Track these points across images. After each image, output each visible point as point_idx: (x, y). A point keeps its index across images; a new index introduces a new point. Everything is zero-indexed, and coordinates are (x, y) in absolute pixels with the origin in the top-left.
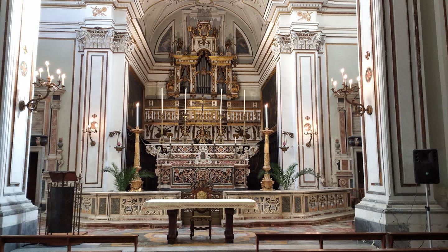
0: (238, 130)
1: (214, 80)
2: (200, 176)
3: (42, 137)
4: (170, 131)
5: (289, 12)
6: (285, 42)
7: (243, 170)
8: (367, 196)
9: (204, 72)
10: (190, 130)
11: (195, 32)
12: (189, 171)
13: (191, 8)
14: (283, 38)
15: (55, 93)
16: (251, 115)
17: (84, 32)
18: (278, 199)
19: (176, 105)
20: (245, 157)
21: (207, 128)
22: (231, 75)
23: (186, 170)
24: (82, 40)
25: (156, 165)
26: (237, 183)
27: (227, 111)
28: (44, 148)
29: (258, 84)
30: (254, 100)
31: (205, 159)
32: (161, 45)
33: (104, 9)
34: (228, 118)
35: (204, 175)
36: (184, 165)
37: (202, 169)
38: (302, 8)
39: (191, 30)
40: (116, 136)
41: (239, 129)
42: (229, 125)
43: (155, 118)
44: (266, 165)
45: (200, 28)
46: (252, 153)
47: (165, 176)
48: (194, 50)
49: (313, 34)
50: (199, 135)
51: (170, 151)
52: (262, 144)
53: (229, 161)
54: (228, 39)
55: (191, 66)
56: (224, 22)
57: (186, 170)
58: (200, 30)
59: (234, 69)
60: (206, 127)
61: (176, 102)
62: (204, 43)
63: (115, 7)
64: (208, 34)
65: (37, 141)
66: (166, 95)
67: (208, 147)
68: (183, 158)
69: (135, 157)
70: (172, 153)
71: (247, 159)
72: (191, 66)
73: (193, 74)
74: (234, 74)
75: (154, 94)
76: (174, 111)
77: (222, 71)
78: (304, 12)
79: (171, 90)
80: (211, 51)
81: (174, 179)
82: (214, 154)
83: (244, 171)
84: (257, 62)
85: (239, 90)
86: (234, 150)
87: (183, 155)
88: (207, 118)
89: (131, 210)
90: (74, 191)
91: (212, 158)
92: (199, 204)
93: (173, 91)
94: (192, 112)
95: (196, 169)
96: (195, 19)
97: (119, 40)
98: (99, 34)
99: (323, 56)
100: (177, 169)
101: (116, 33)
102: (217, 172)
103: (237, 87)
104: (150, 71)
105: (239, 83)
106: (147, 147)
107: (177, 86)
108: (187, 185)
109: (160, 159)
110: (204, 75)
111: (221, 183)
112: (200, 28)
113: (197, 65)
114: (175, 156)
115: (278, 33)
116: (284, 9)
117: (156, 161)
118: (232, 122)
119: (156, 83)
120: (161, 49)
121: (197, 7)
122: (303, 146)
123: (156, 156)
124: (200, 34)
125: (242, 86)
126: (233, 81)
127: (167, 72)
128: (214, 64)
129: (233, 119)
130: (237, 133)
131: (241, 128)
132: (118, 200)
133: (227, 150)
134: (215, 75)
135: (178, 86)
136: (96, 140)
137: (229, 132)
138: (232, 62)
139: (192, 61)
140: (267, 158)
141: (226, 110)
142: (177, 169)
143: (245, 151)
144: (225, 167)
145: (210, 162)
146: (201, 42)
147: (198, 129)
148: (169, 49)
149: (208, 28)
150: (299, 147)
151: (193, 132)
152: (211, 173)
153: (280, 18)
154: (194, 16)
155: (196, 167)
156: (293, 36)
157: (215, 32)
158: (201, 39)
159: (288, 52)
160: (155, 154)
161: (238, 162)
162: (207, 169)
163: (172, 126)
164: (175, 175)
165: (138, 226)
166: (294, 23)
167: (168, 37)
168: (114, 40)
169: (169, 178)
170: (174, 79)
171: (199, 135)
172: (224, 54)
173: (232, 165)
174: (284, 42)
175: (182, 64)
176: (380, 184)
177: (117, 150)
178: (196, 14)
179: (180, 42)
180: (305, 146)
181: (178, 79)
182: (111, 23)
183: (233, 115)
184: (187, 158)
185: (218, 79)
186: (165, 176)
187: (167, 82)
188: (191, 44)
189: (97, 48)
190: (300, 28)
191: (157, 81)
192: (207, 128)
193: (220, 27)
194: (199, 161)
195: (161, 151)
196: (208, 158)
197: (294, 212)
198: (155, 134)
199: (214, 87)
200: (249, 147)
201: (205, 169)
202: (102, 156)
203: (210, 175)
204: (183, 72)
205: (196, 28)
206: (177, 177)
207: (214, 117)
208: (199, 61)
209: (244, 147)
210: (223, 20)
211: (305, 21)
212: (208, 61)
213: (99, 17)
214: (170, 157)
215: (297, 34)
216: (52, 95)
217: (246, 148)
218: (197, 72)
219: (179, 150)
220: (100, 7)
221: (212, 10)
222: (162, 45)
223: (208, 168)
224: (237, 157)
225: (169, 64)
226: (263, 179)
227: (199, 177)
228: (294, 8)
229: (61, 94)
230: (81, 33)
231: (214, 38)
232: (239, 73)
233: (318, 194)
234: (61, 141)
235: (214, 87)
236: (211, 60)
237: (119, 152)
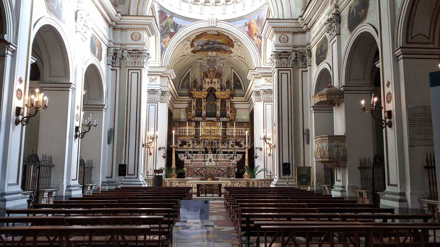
1: (218, 108)
2: (209, 172)
5: (260, 78)
6: (258, 95)
7: (233, 169)
10: (202, 141)
11: (206, 75)
12: (202, 169)
13: (203, 59)
14: (257, 93)
16: (243, 131)
18: (244, 182)
19: (193, 125)
20: (234, 162)
21: (213, 141)
22: (230, 105)
25: (184, 166)
26: (229, 176)
27: (227, 129)
29: (248, 110)
30: (246, 121)
32: (182, 84)
33: (156, 79)
38: (267, 76)
39: (203, 75)
42: (228, 138)
43: (179, 134)
45: (209, 73)
46: (238, 159)
47: (189, 172)
48: (205, 88)
50: (208, 145)
51: (192, 158)
54: (228, 80)
55: (203, 98)
56: (225, 67)
58: (209, 75)
59: (232, 100)
60: (213, 140)
61: (193, 123)
62: (211, 83)
63: (161, 76)
64: (214, 77)
66: (186, 118)
67: (213, 156)
68: (199, 162)
69: (173, 161)
70: (193, 159)
71: (236, 163)
72: (203, 98)
73: (204, 104)
74: (232, 104)
75: (178, 117)
76: (191, 129)
77: (223, 101)
79: (189, 115)
80: (216, 88)
81: (195, 174)
82: (216, 159)
84: (248, 94)
85: (235, 114)
86: (228, 157)
87: (199, 160)
88: (213, 134)
91: (215, 162)
92: (208, 182)
93: (191, 115)
94: (204, 130)
96: (205, 65)
97: (163, 95)
98: (153, 93)
100: (196, 168)
101: (162, 92)
103: (234, 113)
104: (175, 102)
106: (179, 155)
109: (186, 162)
112: (209, 73)
113: (207, 98)
115: (273, 51)
116: (257, 76)
118: (230, 137)
119: (179, 110)
120: (182, 87)
121: (207, 58)
124: (209, 77)
125: (237, 111)
126: (231, 108)
127: (187, 102)
128: (218, 97)
129: (231, 134)
131: (236, 140)
132: (172, 182)
133: (224, 158)
134: (219, 104)
135: (194, 112)
136: (152, 152)
137: (228, 143)
138: (230, 95)
139: (203, 95)
140: (247, 162)
141: (226, 129)
142: (196, 168)
143: (235, 158)
145: (214, 164)
146: (209, 82)
147: (207, 141)
148: (188, 87)
149: (214, 73)
150: (264, 156)
151: (204, 143)
153: (256, 80)
154: (205, 63)
156: (262, 92)
157: (219, 75)
158: (210, 80)
159: (259, 101)
161: (230, 164)
163: (190, 139)
166: (263, 85)
167: (187, 78)
168: (162, 95)
169: (191, 173)
170: (191, 108)
171: (208, 145)
172: (225, 90)
173: (227, 166)
174: (257, 95)
175: (196, 97)
177: (163, 158)
178: (206, 62)
179: (195, 82)
180: (268, 155)
181: (194, 108)
182: (159, 87)
183: (231, 131)
184: (201, 162)
185: (221, 107)
186: (189, 172)
188: (203, 83)
189: (152, 101)
190: (266, 88)
191: (180, 109)
192: (213, 141)
193: (222, 72)
194: (208, 164)
196: (213, 162)
198: (179, 144)
199: (218, 113)
200: (237, 156)
202: (155, 161)
204: (198, 103)
205: (206, 73)
206: (196, 172)
207: (218, 133)
208: (208, 95)
209: (234, 155)
210: (225, 66)
212: (214, 95)
213: (153, 83)
214: (192, 161)
215: (264, 91)
217: (235, 156)
218: (207, 103)
219: (197, 157)
220: (153, 77)
221: (217, 59)
222: (183, 84)
224: (230, 162)
225: (188, 97)
231: (218, 79)
232: (235, 103)
233: (265, 181)
235: (218, 113)
236: (216, 94)
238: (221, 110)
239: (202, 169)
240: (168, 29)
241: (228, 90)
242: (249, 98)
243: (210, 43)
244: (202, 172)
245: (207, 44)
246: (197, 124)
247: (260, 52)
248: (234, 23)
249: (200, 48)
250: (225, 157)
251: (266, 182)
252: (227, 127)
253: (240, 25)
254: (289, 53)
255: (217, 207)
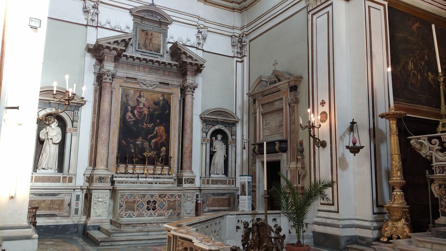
3: (281, 142)
15: (291, 83)
28: (285, 155)
65: (276, 147)
106: (412, 142)
123: (432, 157)
160: (428, 154)
195: (439, 148)
197: (33, 181)
216: (288, 87)
229: (297, 83)
234: (301, 144)
237: (355, 155)
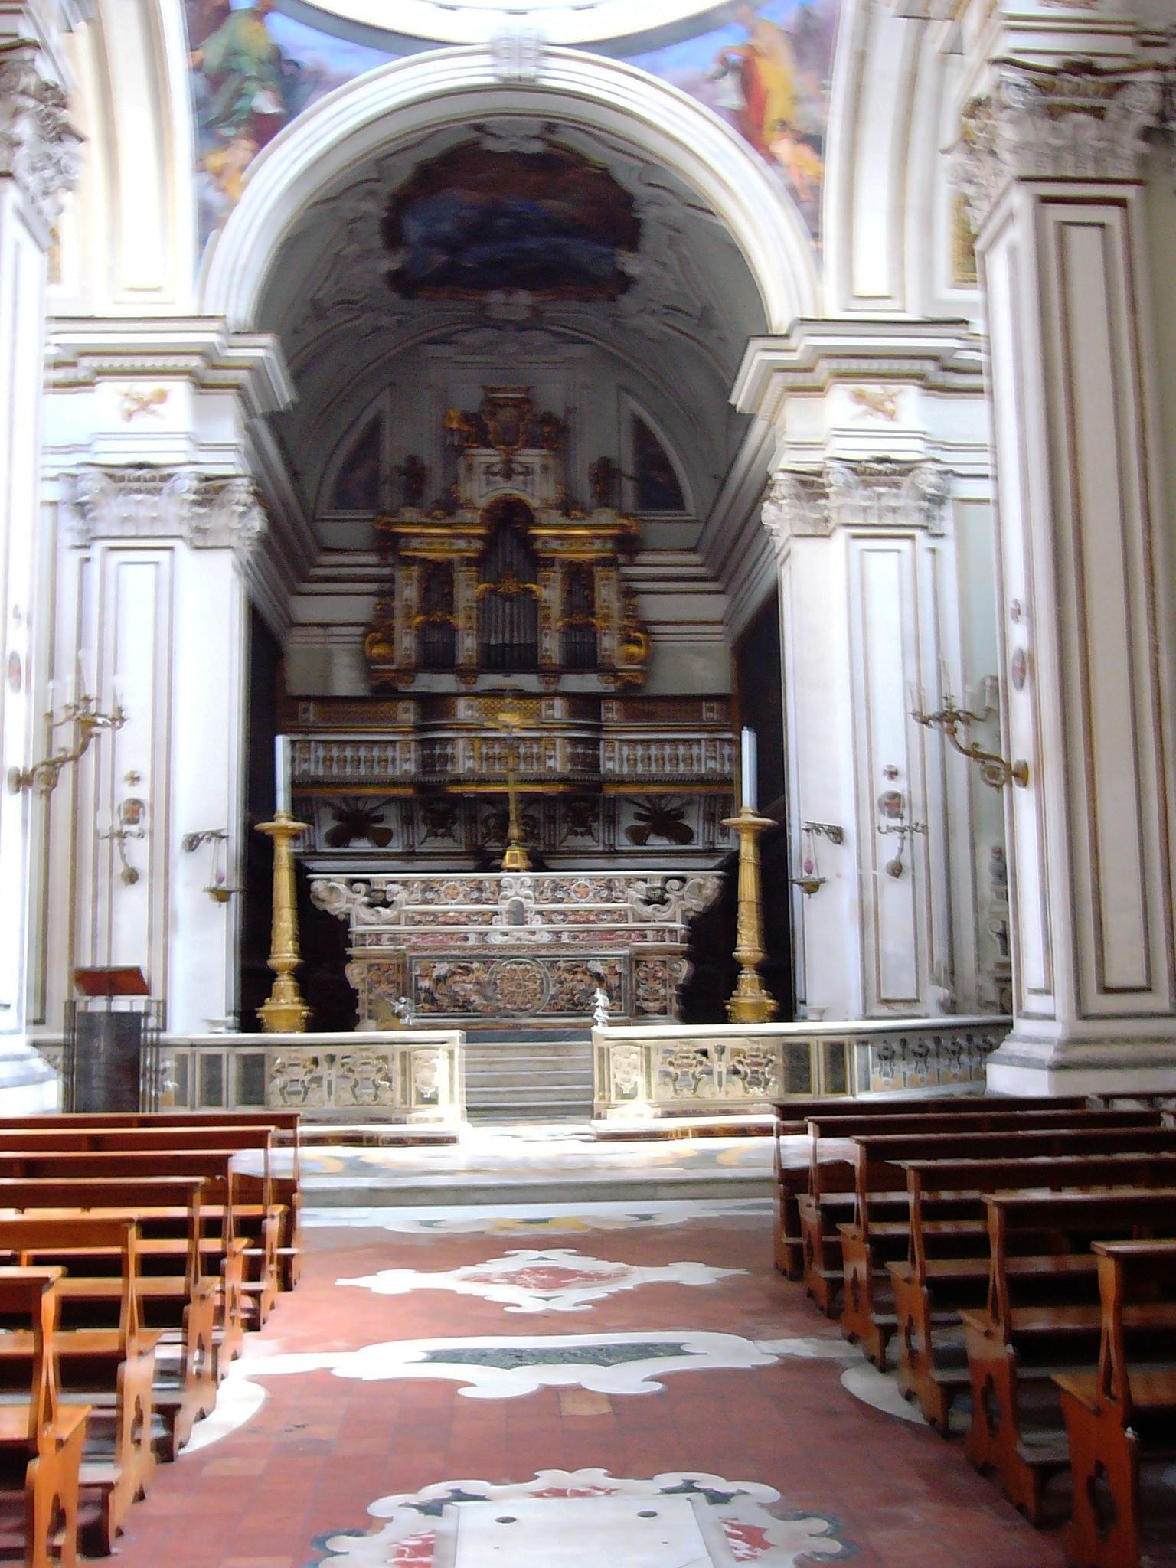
0: (646, 809)
4: (380, 819)
8: (1021, 1027)
9: (511, 587)
17: (92, 484)
20: (673, 919)
23: (461, 968)
24: (81, 509)
31: (526, 926)
33: (161, 397)
34: (608, 766)
35: (521, 982)
36: (450, 948)
37: (515, 963)
40: (207, 848)
41: (647, 805)
44: (748, 945)
46: (696, 904)
49: (908, 468)
52: (731, 866)
53: (612, 932)
57: (461, 968)
61: (402, 705)
73: (467, 591)
77: (579, 578)
78: (873, 389)
80: (534, 503)
83: (665, 966)
89: (302, 1090)
90: (140, 1034)
91: (550, 921)
95: (493, 962)
99: (948, 548)
102: (568, 971)
105: (644, 626)
106: (315, 885)
107: (406, 643)
108: (462, 1020)
110: (509, 598)
111: (584, 1010)
114: (417, 918)
117: (350, 936)
122: (876, 873)
130: (642, 824)
134: (551, 593)
144: (597, 953)
150: (860, 877)
152: (547, 977)
155: (493, 957)
156: (837, 476)
160: (343, 910)
162: (533, 960)
164: (419, 985)
165: (327, 1140)
166: (843, 432)
173: (624, 945)
176: (1047, 991)
180: (883, 874)
181: (408, 617)
182: (184, 445)
187: (370, 627)
190: (863, 449)
194: (506, 934)
196: (537, 923)
199: (552, 646)
201: (525, 963)
203: (542, 983)
208: (491, 542)
211: (879, 422)
212: (527, 542)
213: (142, 422)
220: (146, 387)
223: (538, 959)
225: (372, 559)
226: (735, 993)
227: (506, 992)
228: (843, 376)
230: (83, 485)
233: (903, 1035)
235: (552, 646)
238: (569, 630)
239: (468, 971)
240: (239, 94)
241: (606, 516)
242: (747, 520)
243: (502, 222)
244: (465, 987)
245: (479, 231)
246: (434, 706)
247: (816, 236)
248: (648, 58)
249: (440, 258)
250: (610, 889)
251: (975, 1040)
252: (599, 728)
253: (690, 72)
254: (1112, 79)
255: (628, 1285)
